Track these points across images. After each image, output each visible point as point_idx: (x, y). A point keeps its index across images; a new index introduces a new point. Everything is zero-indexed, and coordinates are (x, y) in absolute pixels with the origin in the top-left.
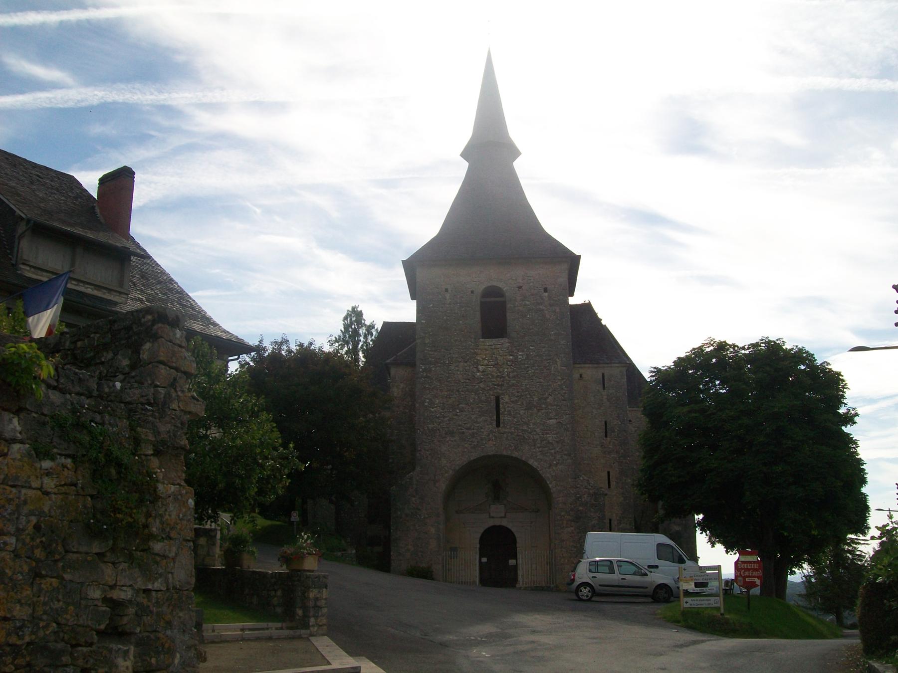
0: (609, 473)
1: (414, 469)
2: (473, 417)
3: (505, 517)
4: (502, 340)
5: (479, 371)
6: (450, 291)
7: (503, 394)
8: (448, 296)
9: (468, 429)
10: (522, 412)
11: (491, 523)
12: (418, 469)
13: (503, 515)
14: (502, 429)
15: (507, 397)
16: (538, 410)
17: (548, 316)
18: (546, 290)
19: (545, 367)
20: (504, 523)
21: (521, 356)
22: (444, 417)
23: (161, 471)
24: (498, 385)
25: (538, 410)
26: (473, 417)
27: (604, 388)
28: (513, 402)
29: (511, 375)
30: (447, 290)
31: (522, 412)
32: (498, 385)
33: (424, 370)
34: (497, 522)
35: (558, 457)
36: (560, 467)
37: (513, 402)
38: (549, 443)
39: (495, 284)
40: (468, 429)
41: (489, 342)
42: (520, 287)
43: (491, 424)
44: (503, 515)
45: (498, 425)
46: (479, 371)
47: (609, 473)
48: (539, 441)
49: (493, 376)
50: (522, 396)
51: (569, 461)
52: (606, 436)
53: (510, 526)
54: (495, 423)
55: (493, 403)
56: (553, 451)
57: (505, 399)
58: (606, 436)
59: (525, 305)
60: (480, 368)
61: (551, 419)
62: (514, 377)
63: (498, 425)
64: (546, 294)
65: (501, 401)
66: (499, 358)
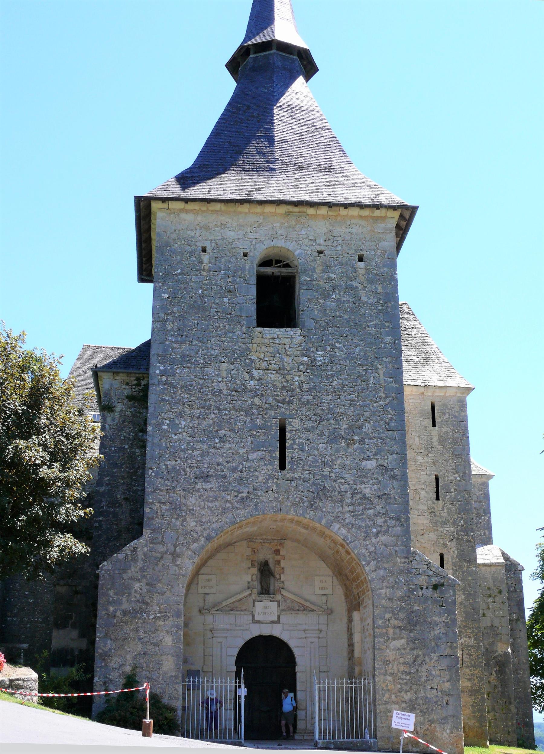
0: (442, 556)
1: (141, 534)
2: (241, 451)
3: (278, 621)
4: (290, 331)
5: (252, 378)
6: (209, 250)
7: (291, 417)
8: (205, 258)
9: (234, 470)
10: (322, 446)
11: (256, 631)
12: (147, 533)
13: (275, 618)
14: (288, 473)
15: (297, 421)
16: (348, 445)
17: (364, 299)
18: (361, 259)
19: (360, 376)
20: (276, 631)
21: (320, 357)
22: (193, 449)
23: (113, 598)
24: (284, 402)
25: (348, 445)
26: (241, 451)
27: (434, 425)
28: (307, 430)
29: (306, 387)
30: (204, 250)
31: (322, 446)
32: (284, 402)
33: (163, 373)
34: (266, 631)
35: (380, 521)
36: (383, 538)
37: (307, 430)
38: (364, 497)
39: (281, 243)
40: (234, 470)
41: (270, 332)
42: (320, 252)
43: (271, 463)
44: (275, 618)
45: (282, 466)
46: (252, 378)
47: (442, 556)
48: (349, 495)
49: (275, 387)
50: (321, 420)
51: (398, 528)
52: (438, 498)
53: (285, 637)
54: (277, 463)
55: (275, 431)
56: (371, 511)
57: (293, 426)
58: (438, 498)
59: (329, 279)
60: (256, 373)
61: (368, 459)
62: (309, 390)
63: (282, 466)
64: (362, 264)
65: (288, 428)
66: (286, 359)
